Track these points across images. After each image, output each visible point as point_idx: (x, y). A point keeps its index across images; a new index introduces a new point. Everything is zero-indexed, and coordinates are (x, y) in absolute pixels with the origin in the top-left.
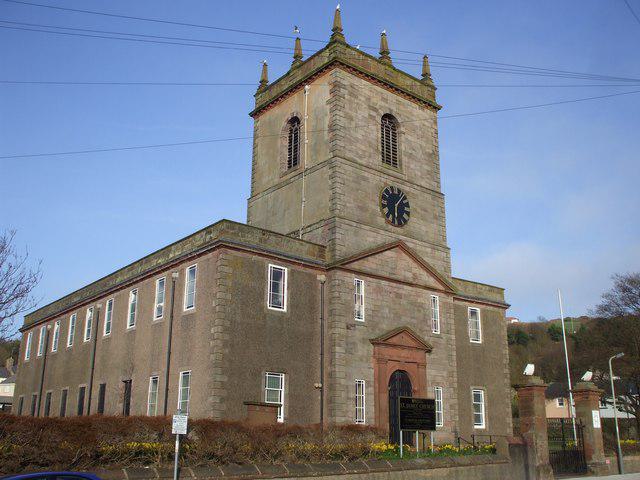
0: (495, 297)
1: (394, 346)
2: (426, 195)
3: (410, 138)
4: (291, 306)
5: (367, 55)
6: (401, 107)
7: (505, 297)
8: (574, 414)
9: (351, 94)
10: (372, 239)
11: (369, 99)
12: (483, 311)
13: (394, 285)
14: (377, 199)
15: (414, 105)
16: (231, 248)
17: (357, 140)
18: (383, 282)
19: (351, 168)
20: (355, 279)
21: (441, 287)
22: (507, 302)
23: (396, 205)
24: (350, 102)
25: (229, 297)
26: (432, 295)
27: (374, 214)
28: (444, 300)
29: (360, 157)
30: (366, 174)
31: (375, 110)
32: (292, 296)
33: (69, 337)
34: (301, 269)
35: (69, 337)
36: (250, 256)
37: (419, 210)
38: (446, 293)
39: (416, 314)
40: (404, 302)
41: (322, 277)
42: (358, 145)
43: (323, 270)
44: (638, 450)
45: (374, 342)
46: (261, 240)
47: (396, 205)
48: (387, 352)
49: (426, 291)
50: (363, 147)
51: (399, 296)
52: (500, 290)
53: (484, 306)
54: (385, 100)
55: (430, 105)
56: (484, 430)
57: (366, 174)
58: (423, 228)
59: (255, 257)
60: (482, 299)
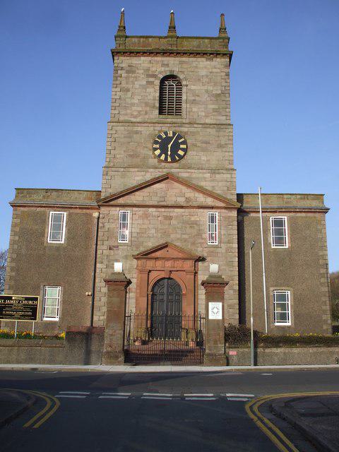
0: (314, 204)
1: (156, 259)
2: (208, 130)
3: (193, 87)
4: (68, 238)
5: (147, 37)
6: (185, 66)
7: (325, 202)
8: (134, 310)
9: (128, 72)
10: (141, 178)
11: (148, 70)
12: (290, 219)
13: (163, 210)
14: (150, 145)
15: (199, 59)
16: (18, 206)
17: (133, 105)
18: (150, 210)
19: (122, 128)
20: (121, 211)
21: (222, 205)
22: (327, 206)
23: (169, 146)
24: (127, 78)
25: (17, 238)
26: (208, 212)
27: (145, 158)
28: (223, 215)
29: (135, 117)
30: (139, 129)
31: (154, 76)
32: (69, 231)
33: (54, 242)
34: (78, 211)
35: (54, 242)
36: (35, 209)
37: (199, 144)
38: (225, 208)
39: (189, 230)
40: (173, 222)
41: (96, 214)
42: (134, 108)
43: (94, 209)
44: (337, 343)
45: (137, 258)
46: (44, 197)
47: (169, 146)
48: (150, 264)
49: (202, 210)
50: (140, 109)
51: (170, 218)
52: (320, 197)
53: (292, 214)
54: (163, 65)
55: (217, 54)
56: (289, 327)
57: (139, 129)
58: (204, 158)
59: (38, 209)
60: (271, 209)
